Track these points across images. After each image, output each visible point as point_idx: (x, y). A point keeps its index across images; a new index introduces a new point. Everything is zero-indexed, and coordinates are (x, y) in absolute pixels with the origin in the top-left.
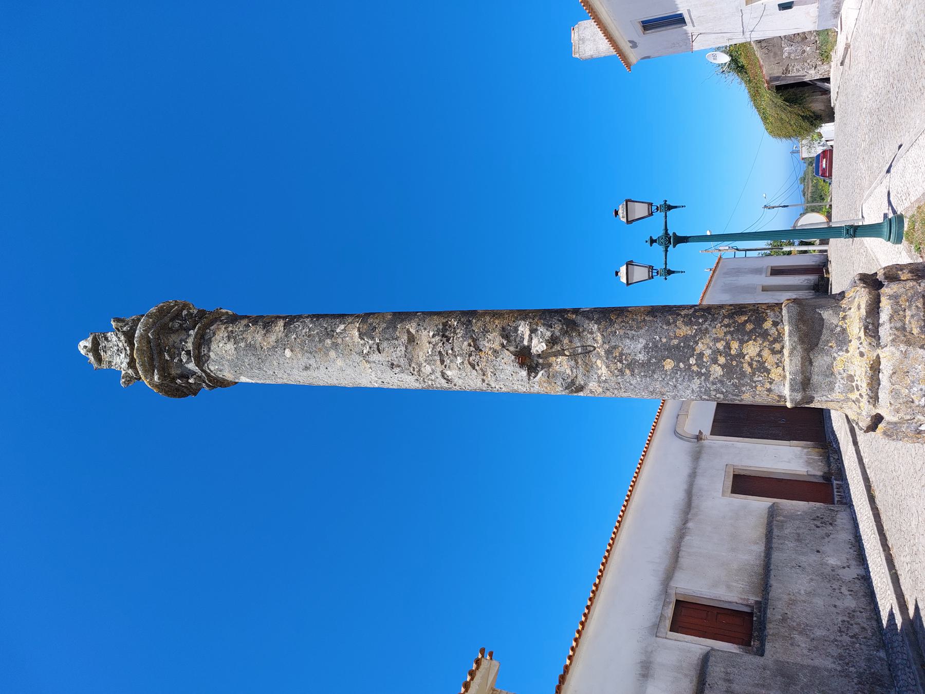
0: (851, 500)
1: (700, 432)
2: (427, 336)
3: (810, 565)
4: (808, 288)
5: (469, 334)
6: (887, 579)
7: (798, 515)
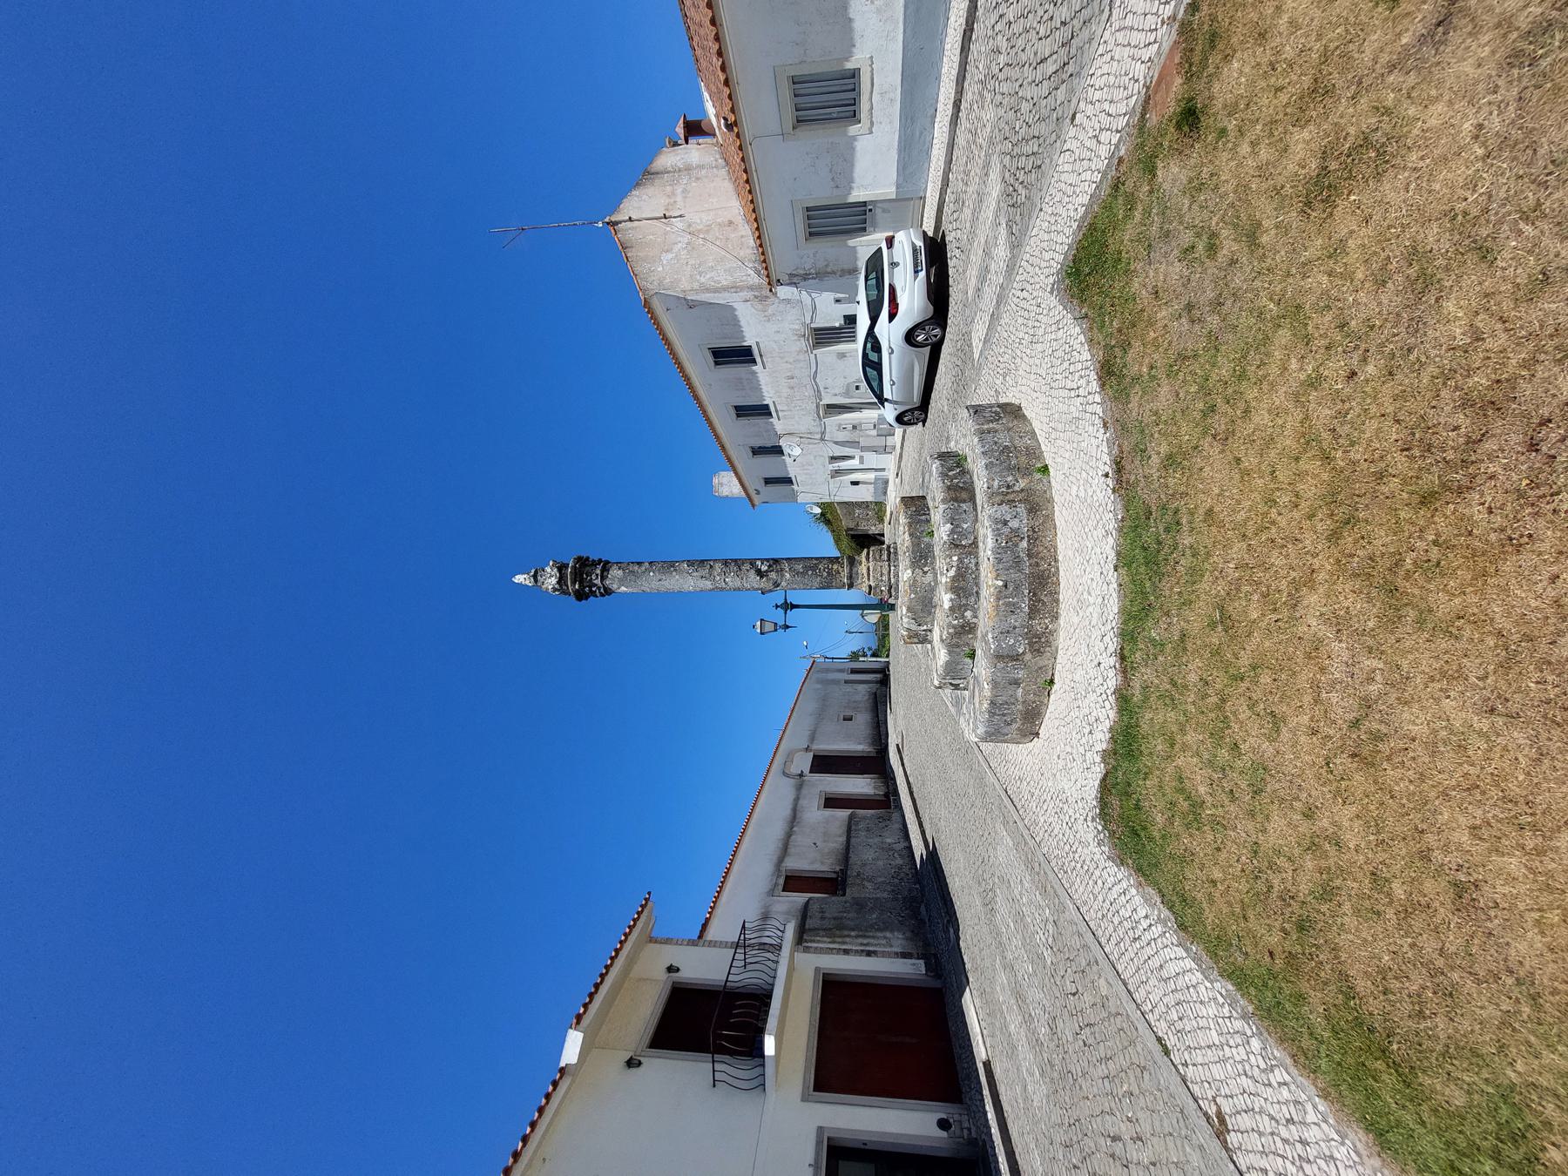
0: (902, 807)
2: (718, 566)
4: (877, 682)
6: (919, 836)
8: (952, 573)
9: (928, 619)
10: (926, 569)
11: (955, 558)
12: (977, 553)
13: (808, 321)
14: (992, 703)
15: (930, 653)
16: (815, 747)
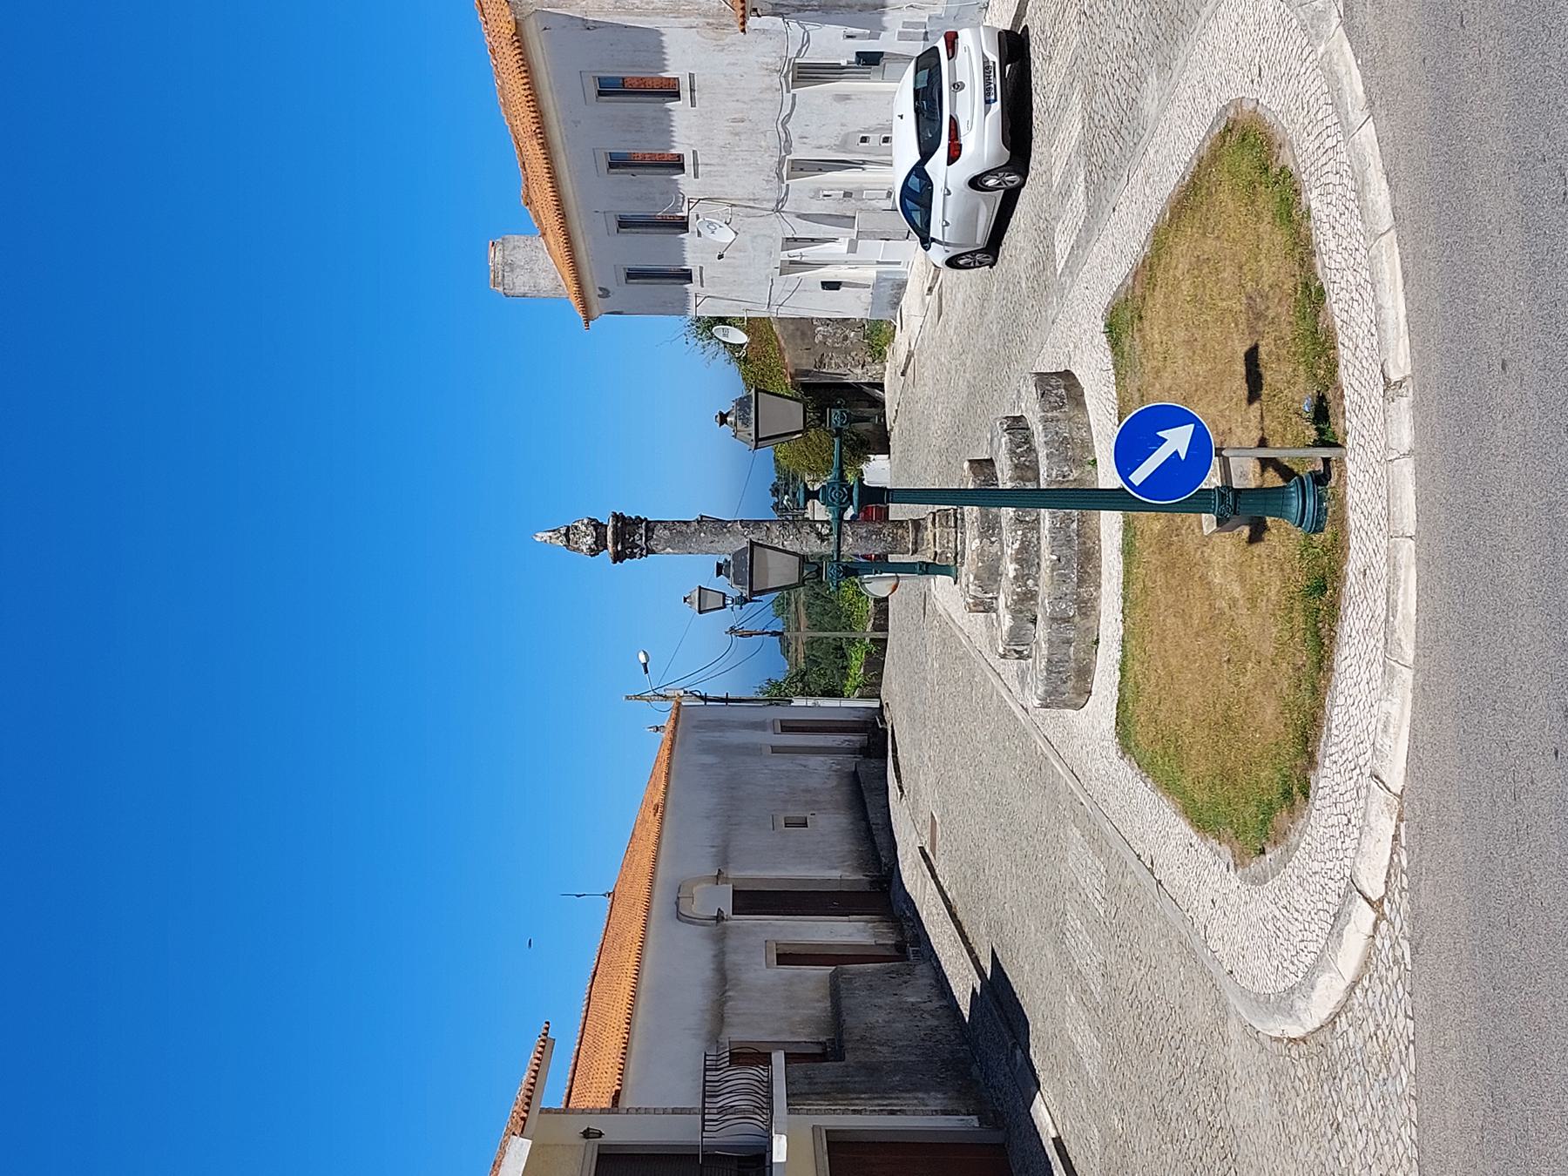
4: (852, 751)
5: (795, 527)
8: (1016, 546)
9: (994, 587)
10: (993, 539)
11: (1020, 533)
12: (1039, 528)
13: (792, 54)
14: (1049, 661)
15: (995, 623)
16: (733, 873)
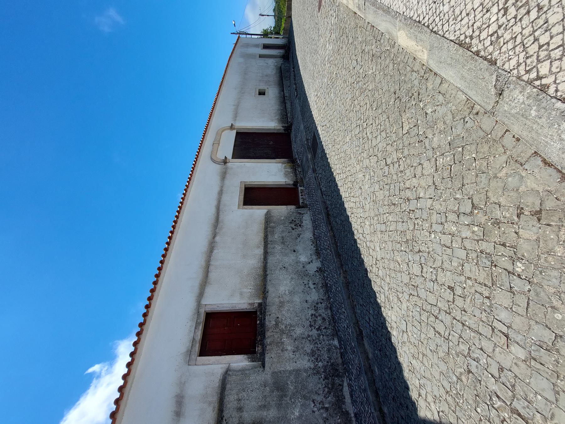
1: (226, 157)
3: (290, 265)
7: (281, 220)
